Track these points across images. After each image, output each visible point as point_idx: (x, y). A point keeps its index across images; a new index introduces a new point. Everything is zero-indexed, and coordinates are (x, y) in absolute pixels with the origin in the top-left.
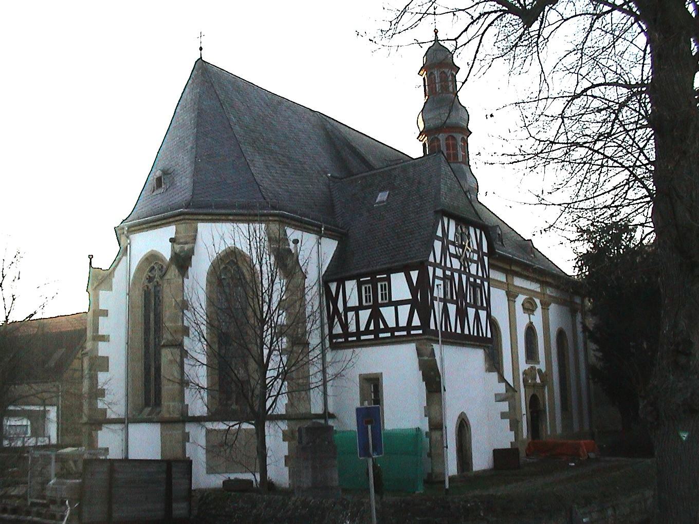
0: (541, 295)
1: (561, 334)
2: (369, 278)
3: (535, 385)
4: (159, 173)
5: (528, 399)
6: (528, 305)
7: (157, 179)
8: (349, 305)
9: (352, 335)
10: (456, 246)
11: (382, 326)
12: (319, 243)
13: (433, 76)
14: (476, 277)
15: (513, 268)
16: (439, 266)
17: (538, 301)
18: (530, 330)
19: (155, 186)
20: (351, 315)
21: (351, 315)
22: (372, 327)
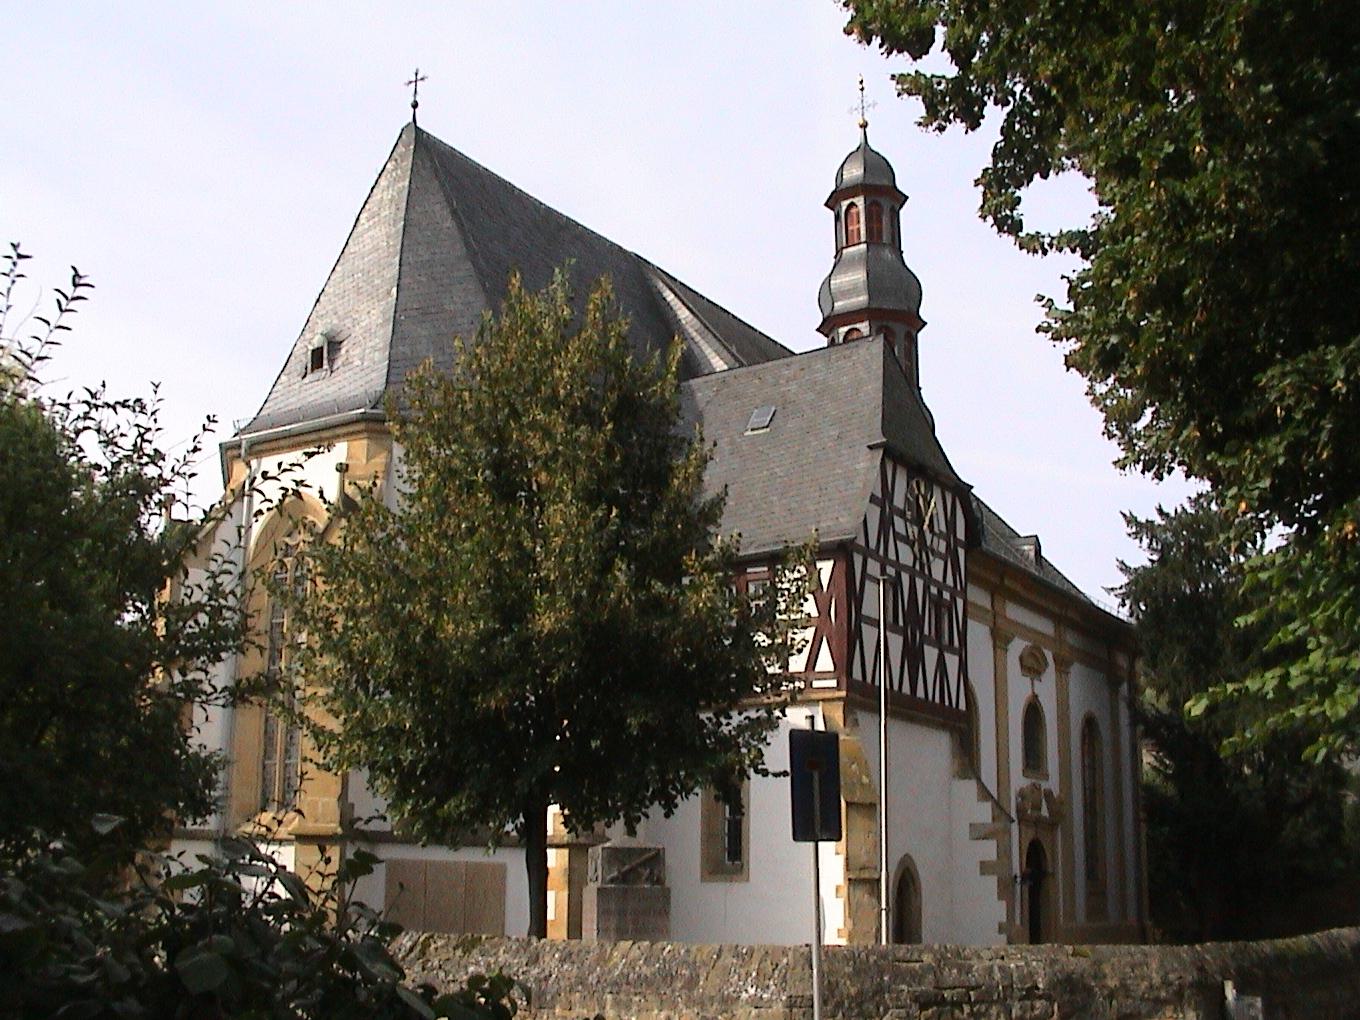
0: (1058, 640)
1: (1090, 723)
3: (1038, 822)
4: (318, 341)
5: (1026, 845)
6: (1030, 662)
7: (313, 351)
10: (906, 520)
14: (942, 587)
16: (875, 554)
18: (1033, 712)
19: (309, 366)
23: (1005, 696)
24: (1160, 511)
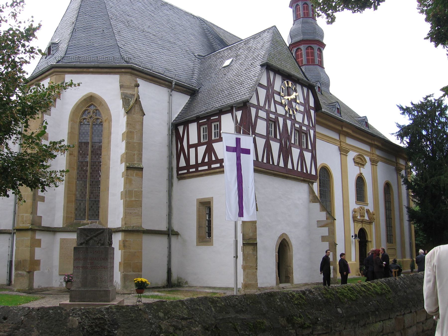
2: (206, 120)
6: (358, 160)
8: (191, 143)
9: (193, 167)
11: (214, 159)
12: (171, 95)
13: (298, 7)
14: (302, 124)
15: (344, 129)
17: (367, 159)
20: (192, 150)
21: (192, 150)
22: (206, 160)
23: (346, 172)
24: (412, 104)
